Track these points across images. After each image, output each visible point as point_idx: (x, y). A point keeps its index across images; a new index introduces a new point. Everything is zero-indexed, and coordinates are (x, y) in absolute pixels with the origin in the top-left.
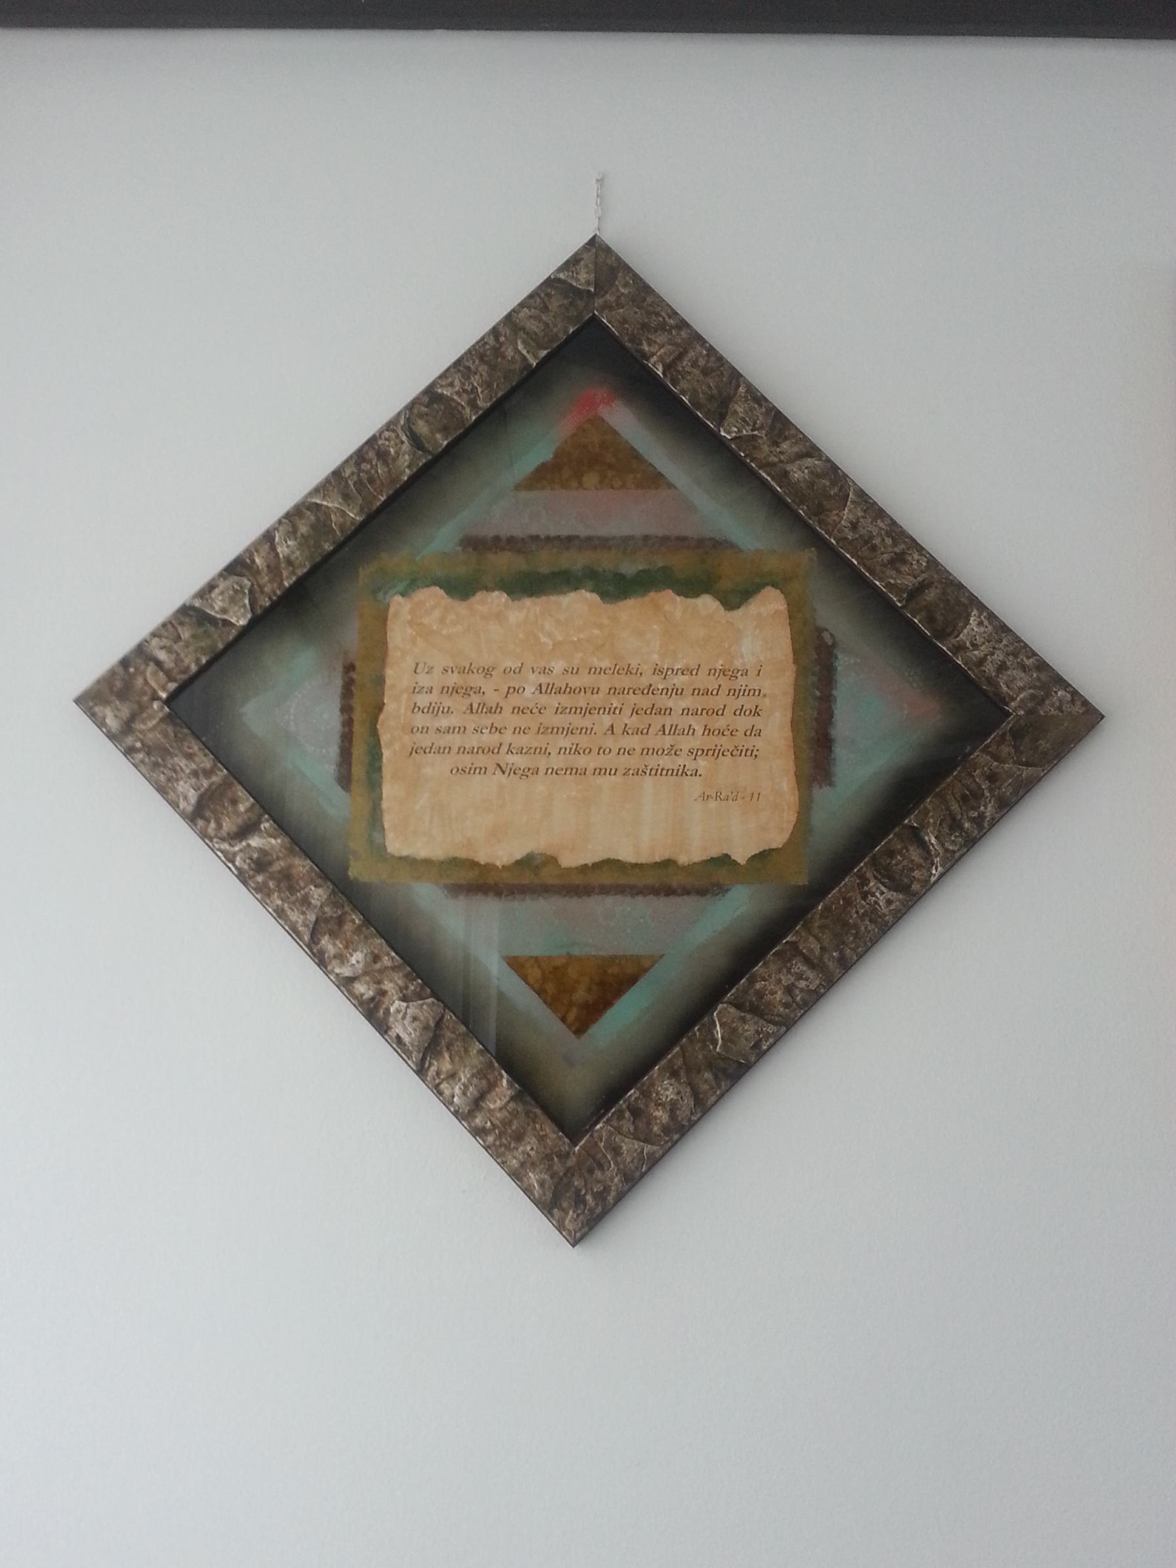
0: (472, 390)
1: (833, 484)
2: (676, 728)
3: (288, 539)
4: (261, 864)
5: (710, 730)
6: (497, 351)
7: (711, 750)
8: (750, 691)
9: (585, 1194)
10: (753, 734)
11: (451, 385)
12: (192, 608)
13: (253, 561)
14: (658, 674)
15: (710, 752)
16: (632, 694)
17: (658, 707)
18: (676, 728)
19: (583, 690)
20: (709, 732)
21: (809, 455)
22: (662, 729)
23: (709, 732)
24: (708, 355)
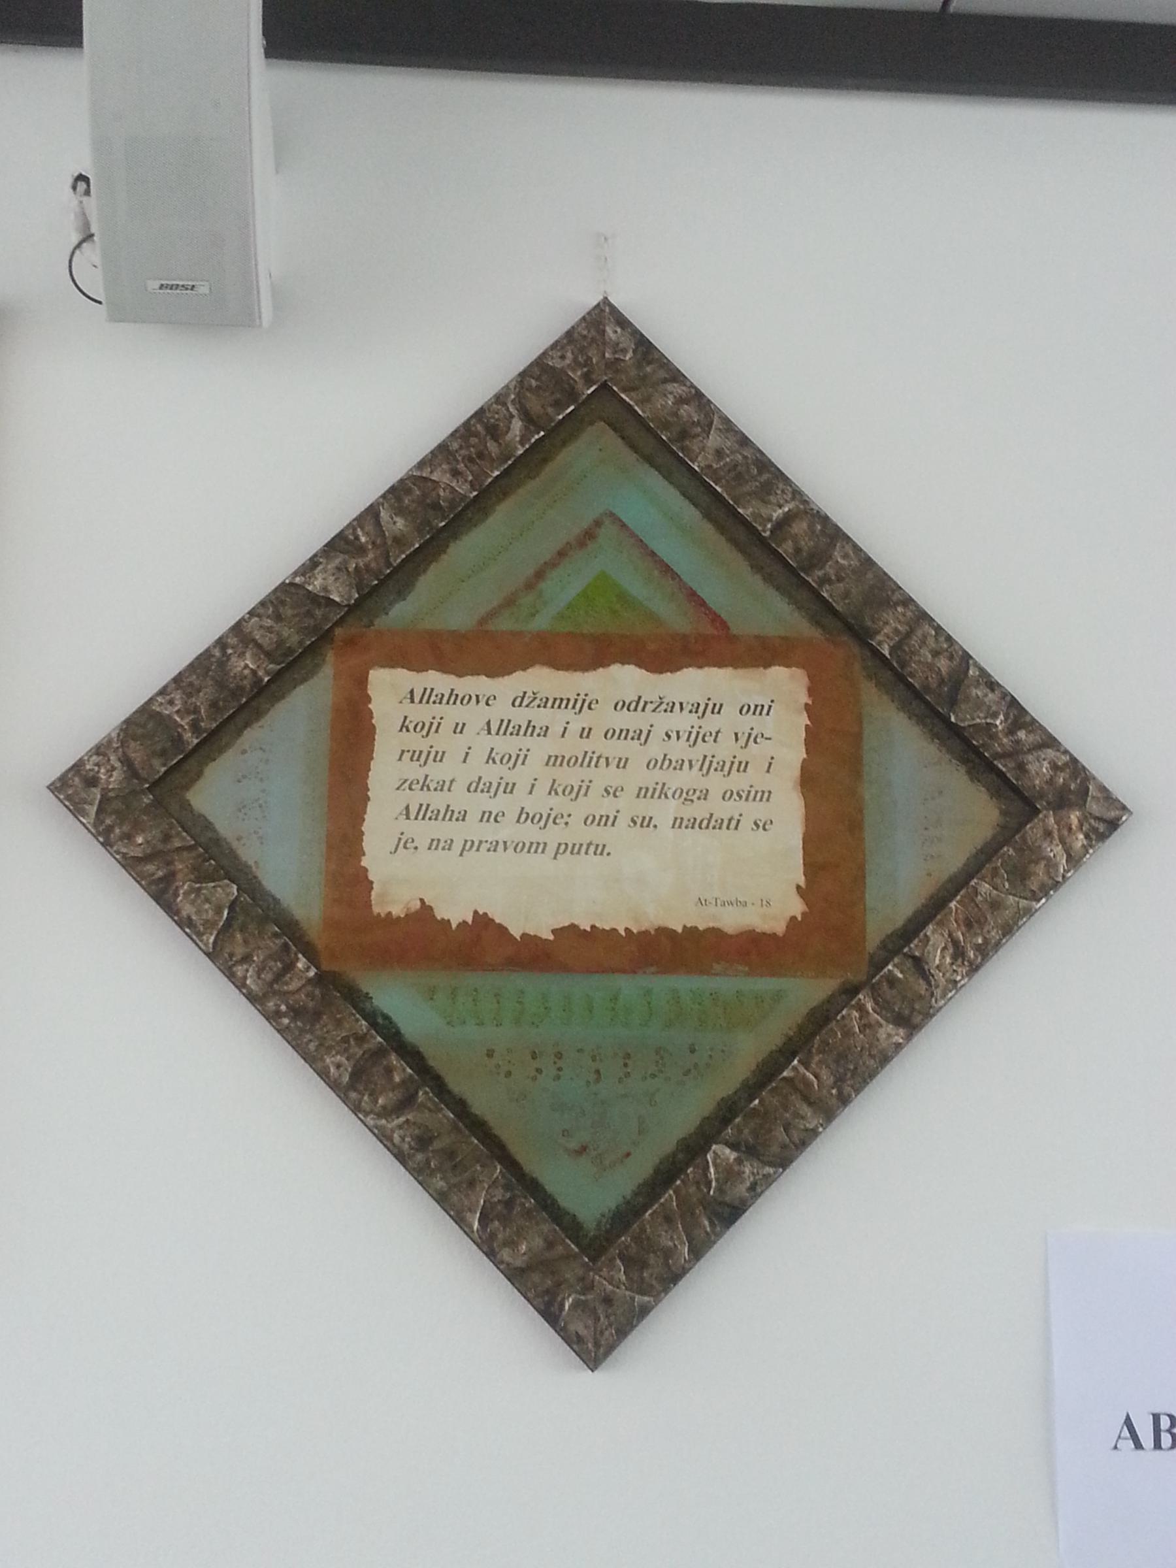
0: (586, 361)
1: (408, 491)
2: (427, 809)
3: (394, 516)
4: (494, 432)
5: (457, 695)
6: (223, 663)
7: (408, 751)
8: (757, 792)
9: (486, 435)
10: (479, 790)
11: (171, 702)
12: (98, 821)
13: (357, 538)
14: (743, 791)
15: (406, 754)
16: (543, 814)
17: (486, 780)
18: (427, 809)
19: (474, 698)
20: (456, 699)
21: (377, 516)
22: (404, 813)
23: (456, 699)
24: (259, 616)
